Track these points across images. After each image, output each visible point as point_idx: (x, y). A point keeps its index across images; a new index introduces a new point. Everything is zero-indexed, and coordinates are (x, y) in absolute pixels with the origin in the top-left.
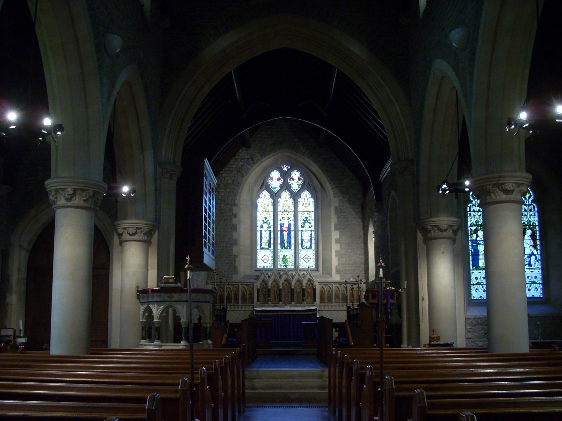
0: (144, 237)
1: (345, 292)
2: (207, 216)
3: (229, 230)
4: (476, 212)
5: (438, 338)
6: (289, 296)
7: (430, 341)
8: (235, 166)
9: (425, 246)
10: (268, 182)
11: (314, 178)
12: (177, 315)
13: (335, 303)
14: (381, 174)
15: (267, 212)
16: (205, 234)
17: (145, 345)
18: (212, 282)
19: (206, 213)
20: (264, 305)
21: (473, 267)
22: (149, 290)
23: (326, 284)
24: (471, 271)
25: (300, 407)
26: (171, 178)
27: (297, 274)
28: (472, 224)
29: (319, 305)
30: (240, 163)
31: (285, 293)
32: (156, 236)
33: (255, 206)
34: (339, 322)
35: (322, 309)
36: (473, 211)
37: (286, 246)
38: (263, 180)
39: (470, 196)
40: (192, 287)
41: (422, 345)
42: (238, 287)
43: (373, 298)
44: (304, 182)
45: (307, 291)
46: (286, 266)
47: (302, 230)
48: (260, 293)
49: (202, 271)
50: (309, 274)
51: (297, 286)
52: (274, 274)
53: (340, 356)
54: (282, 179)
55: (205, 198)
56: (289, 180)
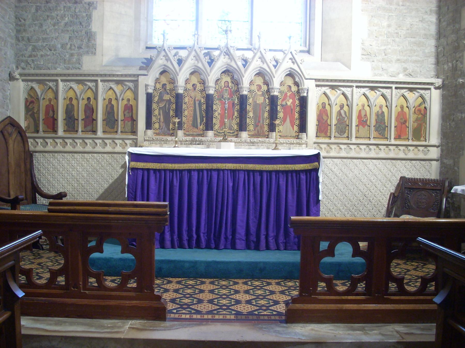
6: (234, 114)
20: (165, 138)
29: (315, 143)
42: (94, 89)
45: (284, 103)
48: (154, 106)
50: (291, 57)
51: (254, 88)
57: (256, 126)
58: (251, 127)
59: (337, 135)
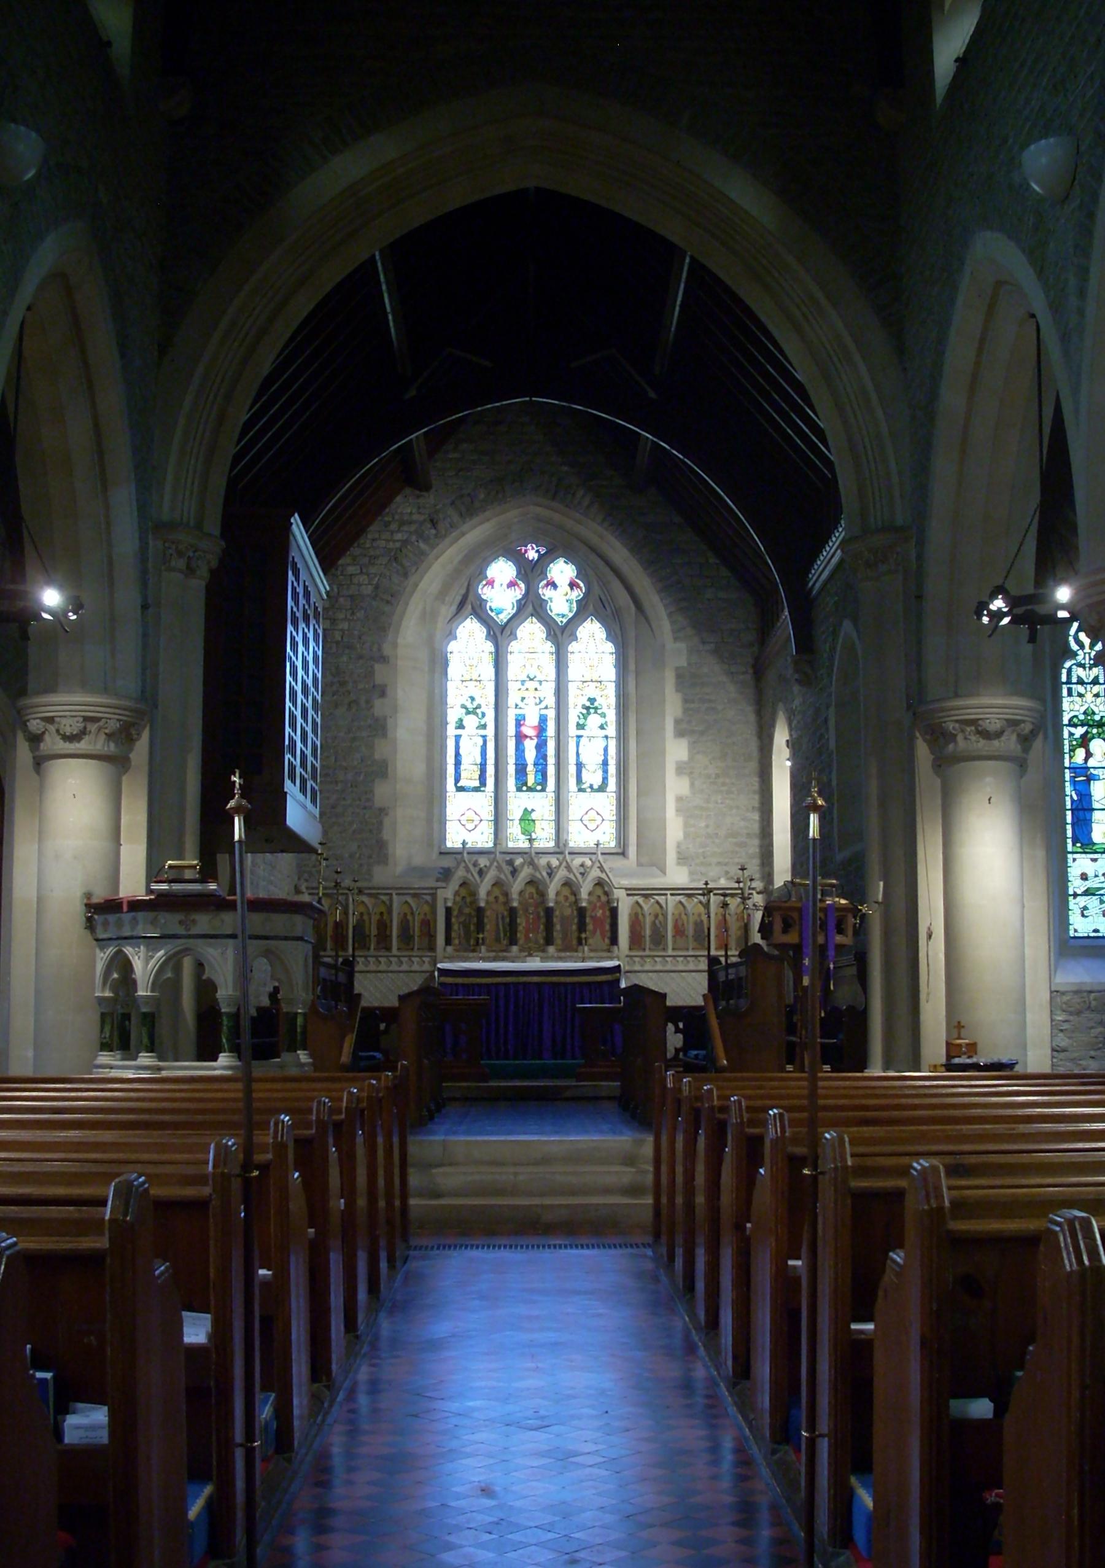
0: (108, 746)
1: (704, 918)
2: (299, 688)
3: (364, 734)
4: (1087, 684)
5: (972, 1048)
6: (539, 928)
7: (949, 1057)
8: (382, 543)
9: (938, 781)
10: (480, 591)
11: (617, 586)
12: (204, 977)
13: (674, 949)
14: (813, 572)
15: (476, 681)
16: (293, 742)
17: (111, 1068)
18: (313, 888)
19: (295, 704)
20: (466, 954)
21: (1074, 844)
22: (122, 903)
23: (647, 894)
24: (1069, 856)
25: (571, 1247)
26: (190, 571)
27: (564, 864)
28: (1075, 720)
29: (627, 956)
30: (399, 536)
31: (528, 921)
32: (142, 745)
33: (439, 664)
34: (685, 1004)
35: (637, 967)
36: (1078, 683)
37: (531, 780)
38: (466, 584)
39: (1071, 639)
40: (249, 894)
41: (927, 1068)
42: (388, 903)
43: (785, 931)
44: (586, 595)
45: (593, 914)
46: (531, 840)
47: (579, 737)
48: (453, 920)
49: (282, 851)
52: (495, 864)
53: (690, 1092)
54: (522, 586)
55: (291, 632)
56: (543, 588)
57: (564, 939)
58: (559, 941)
59: (652, 947)
